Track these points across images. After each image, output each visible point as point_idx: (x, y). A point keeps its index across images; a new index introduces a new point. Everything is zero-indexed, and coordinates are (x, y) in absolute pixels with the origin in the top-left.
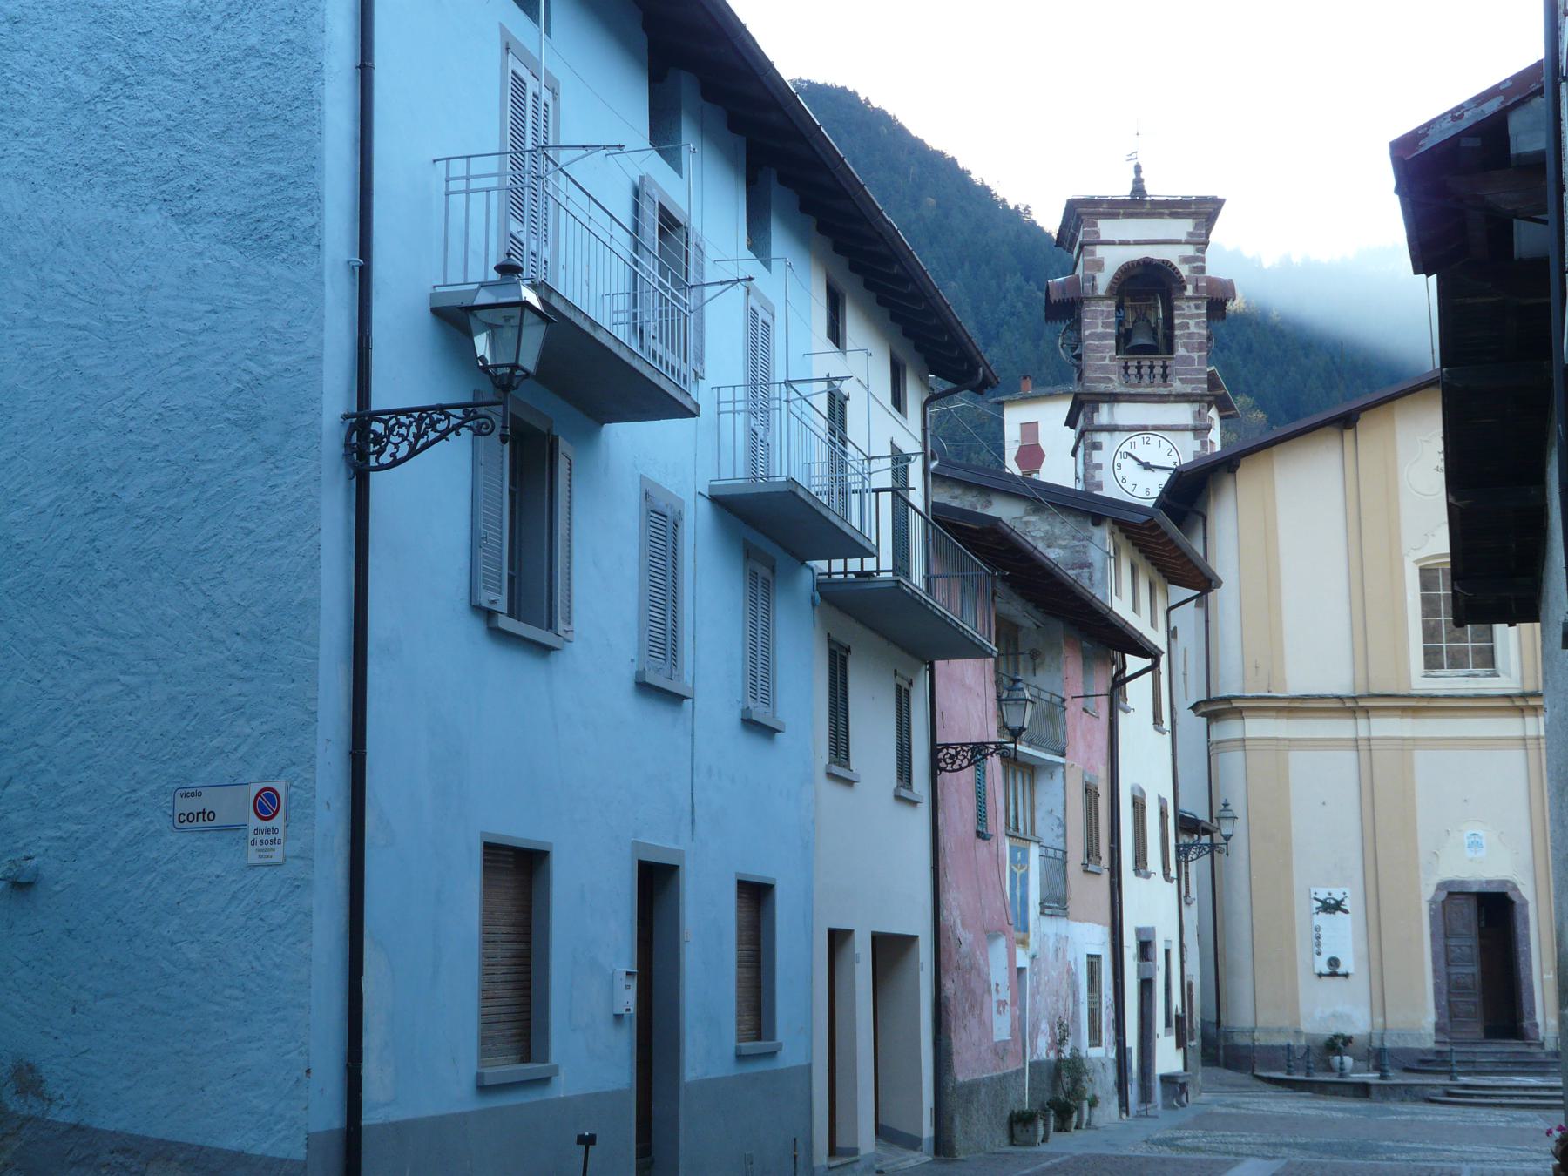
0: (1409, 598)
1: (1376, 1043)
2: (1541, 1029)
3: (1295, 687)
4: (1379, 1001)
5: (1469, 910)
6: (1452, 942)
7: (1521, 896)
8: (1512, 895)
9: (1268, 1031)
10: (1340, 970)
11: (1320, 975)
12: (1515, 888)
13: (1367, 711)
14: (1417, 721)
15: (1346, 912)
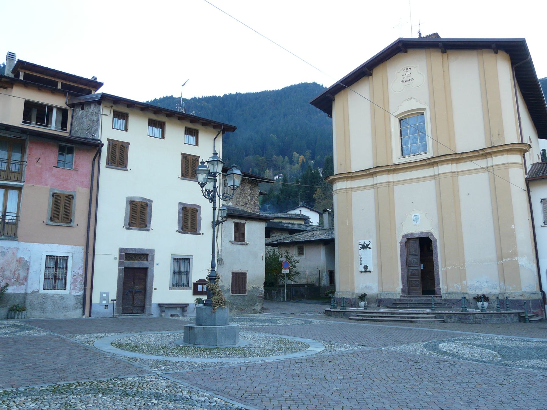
0: (393, 130)
1: (379, 297)
2: (441, 291)
3: (460, 149)
4: (381, 282)
5: (417, 245)
6: (411, 258)
7: (434, 238)
8: (431, 238)
9: (342, 293)
10: (368, 270)
11: (361, 272)
12: (432, 235)
13: (436, 163)
14: (459, 164)
15: (370, 248)
